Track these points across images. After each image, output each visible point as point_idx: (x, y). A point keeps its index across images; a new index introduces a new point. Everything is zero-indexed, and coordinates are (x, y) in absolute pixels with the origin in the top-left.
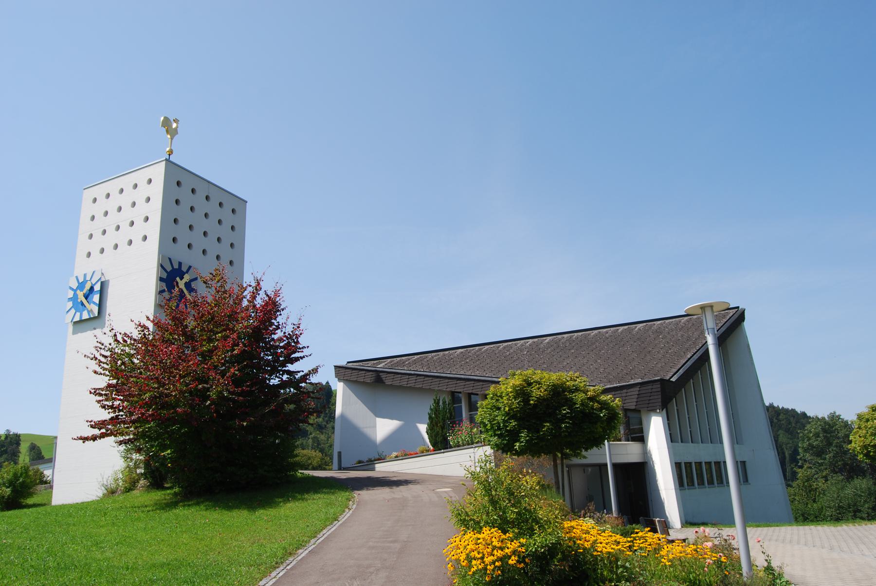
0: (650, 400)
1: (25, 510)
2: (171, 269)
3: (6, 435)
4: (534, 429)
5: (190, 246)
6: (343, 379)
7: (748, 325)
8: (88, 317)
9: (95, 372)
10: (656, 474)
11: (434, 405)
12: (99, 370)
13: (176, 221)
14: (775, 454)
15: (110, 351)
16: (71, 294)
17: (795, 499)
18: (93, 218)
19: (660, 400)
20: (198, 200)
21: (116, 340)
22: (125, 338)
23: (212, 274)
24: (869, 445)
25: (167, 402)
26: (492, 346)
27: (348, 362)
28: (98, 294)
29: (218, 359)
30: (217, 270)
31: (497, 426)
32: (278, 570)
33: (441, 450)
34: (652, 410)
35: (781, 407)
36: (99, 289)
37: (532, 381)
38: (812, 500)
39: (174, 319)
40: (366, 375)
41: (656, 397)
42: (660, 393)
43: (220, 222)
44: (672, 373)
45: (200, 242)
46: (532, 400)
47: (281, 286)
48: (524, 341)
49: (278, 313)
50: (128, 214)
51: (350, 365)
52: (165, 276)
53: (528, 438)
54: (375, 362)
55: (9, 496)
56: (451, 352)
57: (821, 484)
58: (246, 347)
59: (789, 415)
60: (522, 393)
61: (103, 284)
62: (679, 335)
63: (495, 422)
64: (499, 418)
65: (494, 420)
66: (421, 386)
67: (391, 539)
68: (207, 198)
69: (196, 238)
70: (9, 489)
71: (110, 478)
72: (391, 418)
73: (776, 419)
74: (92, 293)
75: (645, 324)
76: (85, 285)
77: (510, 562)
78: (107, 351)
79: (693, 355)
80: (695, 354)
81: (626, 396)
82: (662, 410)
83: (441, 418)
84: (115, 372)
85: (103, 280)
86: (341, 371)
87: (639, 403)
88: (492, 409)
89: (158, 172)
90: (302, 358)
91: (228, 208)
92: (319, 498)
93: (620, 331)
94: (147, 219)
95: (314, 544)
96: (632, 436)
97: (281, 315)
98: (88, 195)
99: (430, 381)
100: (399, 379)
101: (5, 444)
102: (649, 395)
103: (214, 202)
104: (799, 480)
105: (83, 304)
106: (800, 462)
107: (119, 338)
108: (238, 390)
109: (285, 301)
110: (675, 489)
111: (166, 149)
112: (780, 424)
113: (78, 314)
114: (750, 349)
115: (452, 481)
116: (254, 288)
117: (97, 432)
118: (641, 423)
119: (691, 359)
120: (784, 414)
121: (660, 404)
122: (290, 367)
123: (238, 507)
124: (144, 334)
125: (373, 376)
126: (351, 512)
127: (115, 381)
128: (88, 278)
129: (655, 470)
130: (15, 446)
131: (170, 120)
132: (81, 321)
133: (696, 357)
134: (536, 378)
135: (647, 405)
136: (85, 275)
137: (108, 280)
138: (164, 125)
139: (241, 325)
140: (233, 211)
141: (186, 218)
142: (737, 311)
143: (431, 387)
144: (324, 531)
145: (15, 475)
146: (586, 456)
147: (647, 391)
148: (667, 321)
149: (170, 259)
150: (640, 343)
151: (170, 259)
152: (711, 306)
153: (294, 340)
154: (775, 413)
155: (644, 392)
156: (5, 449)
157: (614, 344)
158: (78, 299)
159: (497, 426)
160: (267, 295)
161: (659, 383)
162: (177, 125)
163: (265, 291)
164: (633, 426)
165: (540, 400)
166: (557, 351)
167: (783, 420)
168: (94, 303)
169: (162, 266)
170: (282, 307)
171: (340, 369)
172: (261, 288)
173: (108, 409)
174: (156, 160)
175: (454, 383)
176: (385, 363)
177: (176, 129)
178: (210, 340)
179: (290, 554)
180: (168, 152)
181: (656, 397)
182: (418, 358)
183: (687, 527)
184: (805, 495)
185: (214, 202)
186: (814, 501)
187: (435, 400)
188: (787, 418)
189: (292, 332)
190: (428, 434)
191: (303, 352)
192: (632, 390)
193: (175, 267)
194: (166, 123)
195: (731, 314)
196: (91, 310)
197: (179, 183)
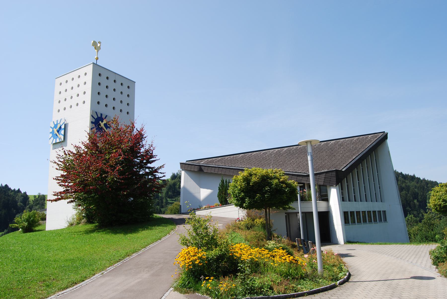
0: (330, 180)
1: (35, 233)
2: (97, 117)
3: (38, 195)
4: (252, 197)
5: (106, 105)
6: (184, 170)
7: (389, 142)
8: (59, 141)
9: (57, 169)
10: (333, 217)
11: (221, 183)
12: (58, 168)
13: (99, 93)
14: (401, 207)
15: (64, 159)
16: (51, 130)
17: (423, 229)
18: (60, 93)
19: (335, 180)
20: (110, 83)
21: (65, 154)
22: (69, 153)
23: (113, 120)
24: (437, 204)
25: (87, 183)
26: (257, 152)
27: (187, 161)
28: (63, 130)
29: (112, 162)
30: (115, 118)
31: (236, 195)
32: (119, 263)
33: (224, 205)
34: (332, 185)
35: (429, 180)
36: (64, 128)
37: (252, 174)
38: (431, 230)
39: (92, 143)
40: (195, 167)
41: (333, 179)
42: (335, 177)
43: (121, 93)
44: (344, 167)
45: (111, 104)
46: (251, 183)
47: (144, 126)
48: (273, 150)
49: (143, 139)
50: (70, 92)
51: (187, 163)
52: (94, 121)
53: (249, 201)
54: (200, 161)
55: (27, 226)
56: (237, 155)
57: (437, 221)
58: (126, 156)
59: (433, 184)
60: (247, 180)
61: (65, 125)
62: (351, 147)
63: (235, 193)
64: (236, 192)
65: (235, 192)
66: (221, 173)
67: (176, 249)
68: (115, 81)
69: (109, 101)
70: (27, 223)
71: (71, 218)
72: (208, 188)
73: (426, 186)
74: (60, 130)
75: (335, 141)
76: (57, 126)
77: (196, 262)
78: (62, 159)
79: (356, 157)
80: (357, 156)
81: (319, 178)
82: (336, 186)
83: (224, 189)
84: (66, 169)
85: (65, 123)
86: (183, 166)
87: (325, 182)
88: (234, 187)
89: (89, 69)
90: (154, 161)
91: (125, 86)
92: (159, 228)
93: (322, 144)
94: (85, 93)
95: (143, 251)
96: (322, 198)
97: (144, 140)
98: (58, 81)
99: (225, 170)
100: (210, 169)
101: (38, 200)
102: (330, 178)
103: (118, 83)
104: (425, 220)
105: (56, 135)
106: (427, 210)
107: (67, 153)
108: (121, 177)
109: (146, 133)
110: (342, 225)
111: (95, 57)
112: (428, 189)
113: (55, 140)
114: (390, 153)
115: (226, 220)
116: (131, 127)
117: (56, 197)
118: (327, 192)
119: (355, 159)
120: (431, 184)
121: (335, 182)
122: (149, 165)
123: (119, 233)
124: (78, 151)
125: (198, 168)
126: (170, 235)
127: (65, 173)
128: (59, 122)
129: (332, 215)
130: (43, 201)
131: (96, 42)
132: (56, 143)
133: (357, 158)
134: (254, 172)
135: (329, 183)
136: (57, 121)
137: (68, 123)
138: (93, 45)
139: (124, 145)
140: (128, 87)
141: (105, 91)
142: (383, 134)
143: (225, 173)
144: (151, 245)
145: (29, 216)
146: (295, 208)
147: (329, 176)
148: (347, 139)
149: (96, 112)
150: (331, 151)
151: (96, 112)
152: (310, 142)
153: (150, 152)
154: (426, 183)
155: (327, 176)
156: (38, 202)
157: (318, 151)
158: (54, 132)
159: (236, 195)
160: (138, 131)
161: (335, 172)
162: (100, 45)
163: (136, 128)
164: (323, 193)
165: (255, 183)
166: (289, 155)
167: (430, 187)
168: (62, 134)
169: (92, 116)
170: (144, 136)
171: (183, 164)
172: (135, 127)
173: (63, 186)
174: (87, 64)
175: (236, 171)
176: (205, 161)
177: (100, 47)
178: (109, 153)
179: (128, 255)
180: (96, 58)
181: (333, 179)
182: (220, 159)
183: (346, 244)
184: (428, 227)
185: (118, 83)
186: (432, 230)
187: (221, 181)
188: (432, 186)
189: (148, 148)
190: (218, 197)
191: (156, 158)
192: (322, 175)
193: (99, 116)
194: (95, 44)
195: (380, 135)
196: (61, 138)
197: (100, 75)
